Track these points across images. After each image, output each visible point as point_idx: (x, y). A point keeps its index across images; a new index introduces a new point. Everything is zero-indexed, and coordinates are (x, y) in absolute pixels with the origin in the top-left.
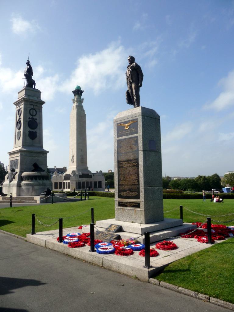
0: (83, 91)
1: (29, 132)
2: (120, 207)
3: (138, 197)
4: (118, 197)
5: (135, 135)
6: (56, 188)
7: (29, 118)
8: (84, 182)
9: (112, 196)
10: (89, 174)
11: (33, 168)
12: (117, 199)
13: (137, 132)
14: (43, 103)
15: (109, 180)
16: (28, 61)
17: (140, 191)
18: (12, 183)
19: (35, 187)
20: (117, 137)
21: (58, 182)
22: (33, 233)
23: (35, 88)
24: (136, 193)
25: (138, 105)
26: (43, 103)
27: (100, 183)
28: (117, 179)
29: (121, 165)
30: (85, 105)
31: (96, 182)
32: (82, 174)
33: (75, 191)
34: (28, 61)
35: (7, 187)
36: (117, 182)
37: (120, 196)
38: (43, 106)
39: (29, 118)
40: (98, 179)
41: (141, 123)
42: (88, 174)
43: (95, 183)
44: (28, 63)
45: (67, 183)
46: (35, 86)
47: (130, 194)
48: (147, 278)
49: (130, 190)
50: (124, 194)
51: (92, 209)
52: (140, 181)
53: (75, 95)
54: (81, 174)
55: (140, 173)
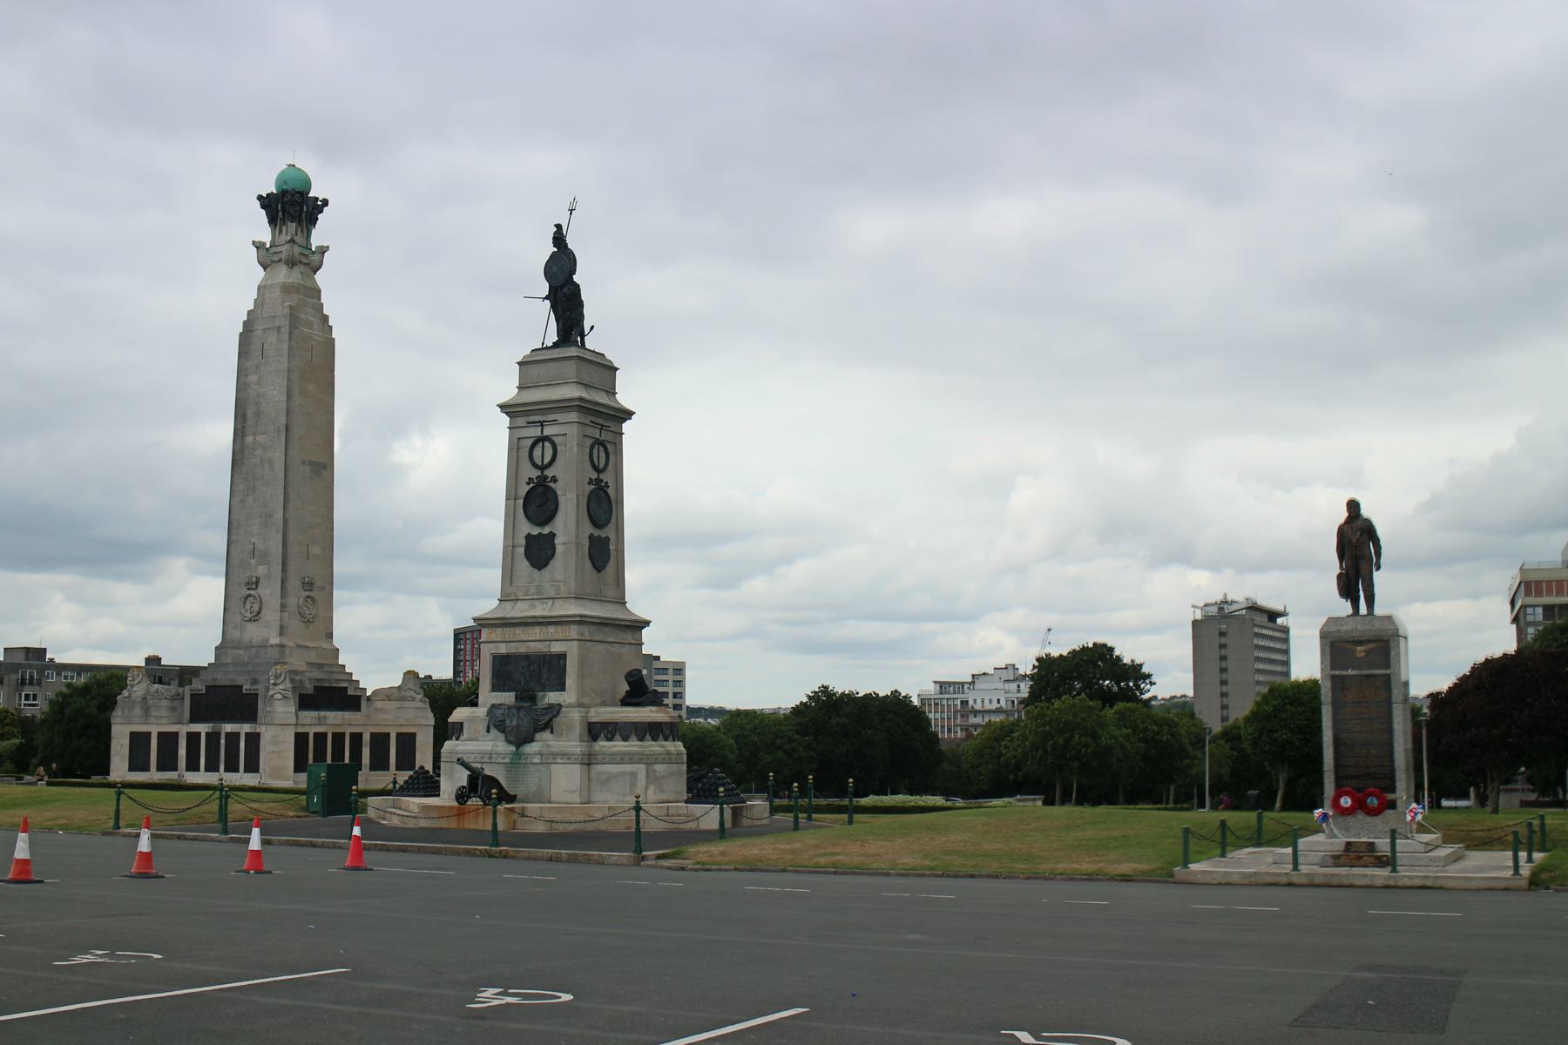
0: (325, 203)
1: (591, 537)
6: (138, 761)
8: (325, 735)
10: (350, 692)
14: (628, 414)
19: (659, 768)
21: (154, 731)
26: (628, 414)
30: (336, 289)
32: (208, 687)
38: (626, 426)
40: (392, 721)
43: (380, 741)
44: (559, 239)
53: (272, 221)
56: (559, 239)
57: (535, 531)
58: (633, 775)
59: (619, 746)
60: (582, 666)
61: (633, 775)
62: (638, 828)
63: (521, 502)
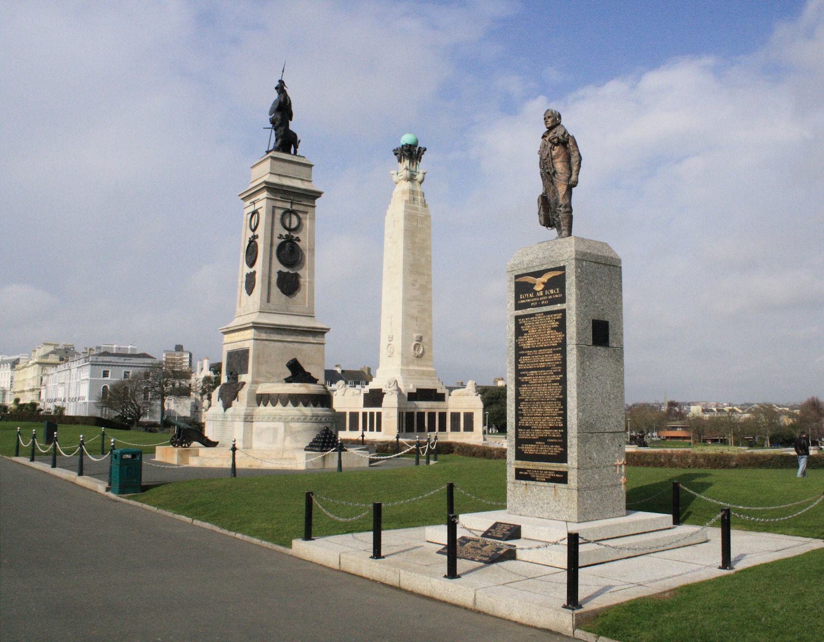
2: (518, 481)
3: (562, 457)
4: (514, 458)
5: (559, 307)
7: (281, 237)
9: (502, 454)
11: (288, 373)
12: (512, 463)
13: (562, 300)
15: (495, 408)
16: (282, 82)
17: (569, 444)
18: (230, 410)
20: (516, 309)
22: (308, 537)
23: (580, 570)
24: (557, 449)
25: (570, 234)
27: (469, 417)
28: (514, 413)
29: (523, 379)
31: (459, 414)
33: (400, 440)
34: (282, 82)
35: (219, 423)
36: (513, 420)
37: (520, 455)
39: (281, 237)
41: (573, 278)
42: (436, 390)
43: (455, 416)
44: (281, 88)
45: (372, 414)
46: (296, 147)
47: (544, 450)
48: (570, 629)
49: (544, 439)
50: (529, 449)
51: (451, 487)
52: (568, 419)
54: (415, 391)
55: (569, 399)
56: (281, 88)
57: (285, 270)
58: (275, 430)
59: (270, 409)
60: (257, 357)
61: (275, 430)
62: (234, 464)
63: (275, 248)
